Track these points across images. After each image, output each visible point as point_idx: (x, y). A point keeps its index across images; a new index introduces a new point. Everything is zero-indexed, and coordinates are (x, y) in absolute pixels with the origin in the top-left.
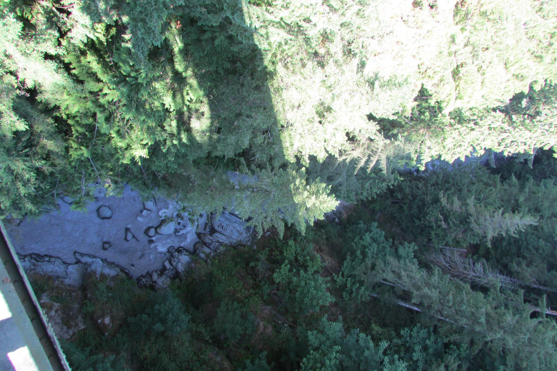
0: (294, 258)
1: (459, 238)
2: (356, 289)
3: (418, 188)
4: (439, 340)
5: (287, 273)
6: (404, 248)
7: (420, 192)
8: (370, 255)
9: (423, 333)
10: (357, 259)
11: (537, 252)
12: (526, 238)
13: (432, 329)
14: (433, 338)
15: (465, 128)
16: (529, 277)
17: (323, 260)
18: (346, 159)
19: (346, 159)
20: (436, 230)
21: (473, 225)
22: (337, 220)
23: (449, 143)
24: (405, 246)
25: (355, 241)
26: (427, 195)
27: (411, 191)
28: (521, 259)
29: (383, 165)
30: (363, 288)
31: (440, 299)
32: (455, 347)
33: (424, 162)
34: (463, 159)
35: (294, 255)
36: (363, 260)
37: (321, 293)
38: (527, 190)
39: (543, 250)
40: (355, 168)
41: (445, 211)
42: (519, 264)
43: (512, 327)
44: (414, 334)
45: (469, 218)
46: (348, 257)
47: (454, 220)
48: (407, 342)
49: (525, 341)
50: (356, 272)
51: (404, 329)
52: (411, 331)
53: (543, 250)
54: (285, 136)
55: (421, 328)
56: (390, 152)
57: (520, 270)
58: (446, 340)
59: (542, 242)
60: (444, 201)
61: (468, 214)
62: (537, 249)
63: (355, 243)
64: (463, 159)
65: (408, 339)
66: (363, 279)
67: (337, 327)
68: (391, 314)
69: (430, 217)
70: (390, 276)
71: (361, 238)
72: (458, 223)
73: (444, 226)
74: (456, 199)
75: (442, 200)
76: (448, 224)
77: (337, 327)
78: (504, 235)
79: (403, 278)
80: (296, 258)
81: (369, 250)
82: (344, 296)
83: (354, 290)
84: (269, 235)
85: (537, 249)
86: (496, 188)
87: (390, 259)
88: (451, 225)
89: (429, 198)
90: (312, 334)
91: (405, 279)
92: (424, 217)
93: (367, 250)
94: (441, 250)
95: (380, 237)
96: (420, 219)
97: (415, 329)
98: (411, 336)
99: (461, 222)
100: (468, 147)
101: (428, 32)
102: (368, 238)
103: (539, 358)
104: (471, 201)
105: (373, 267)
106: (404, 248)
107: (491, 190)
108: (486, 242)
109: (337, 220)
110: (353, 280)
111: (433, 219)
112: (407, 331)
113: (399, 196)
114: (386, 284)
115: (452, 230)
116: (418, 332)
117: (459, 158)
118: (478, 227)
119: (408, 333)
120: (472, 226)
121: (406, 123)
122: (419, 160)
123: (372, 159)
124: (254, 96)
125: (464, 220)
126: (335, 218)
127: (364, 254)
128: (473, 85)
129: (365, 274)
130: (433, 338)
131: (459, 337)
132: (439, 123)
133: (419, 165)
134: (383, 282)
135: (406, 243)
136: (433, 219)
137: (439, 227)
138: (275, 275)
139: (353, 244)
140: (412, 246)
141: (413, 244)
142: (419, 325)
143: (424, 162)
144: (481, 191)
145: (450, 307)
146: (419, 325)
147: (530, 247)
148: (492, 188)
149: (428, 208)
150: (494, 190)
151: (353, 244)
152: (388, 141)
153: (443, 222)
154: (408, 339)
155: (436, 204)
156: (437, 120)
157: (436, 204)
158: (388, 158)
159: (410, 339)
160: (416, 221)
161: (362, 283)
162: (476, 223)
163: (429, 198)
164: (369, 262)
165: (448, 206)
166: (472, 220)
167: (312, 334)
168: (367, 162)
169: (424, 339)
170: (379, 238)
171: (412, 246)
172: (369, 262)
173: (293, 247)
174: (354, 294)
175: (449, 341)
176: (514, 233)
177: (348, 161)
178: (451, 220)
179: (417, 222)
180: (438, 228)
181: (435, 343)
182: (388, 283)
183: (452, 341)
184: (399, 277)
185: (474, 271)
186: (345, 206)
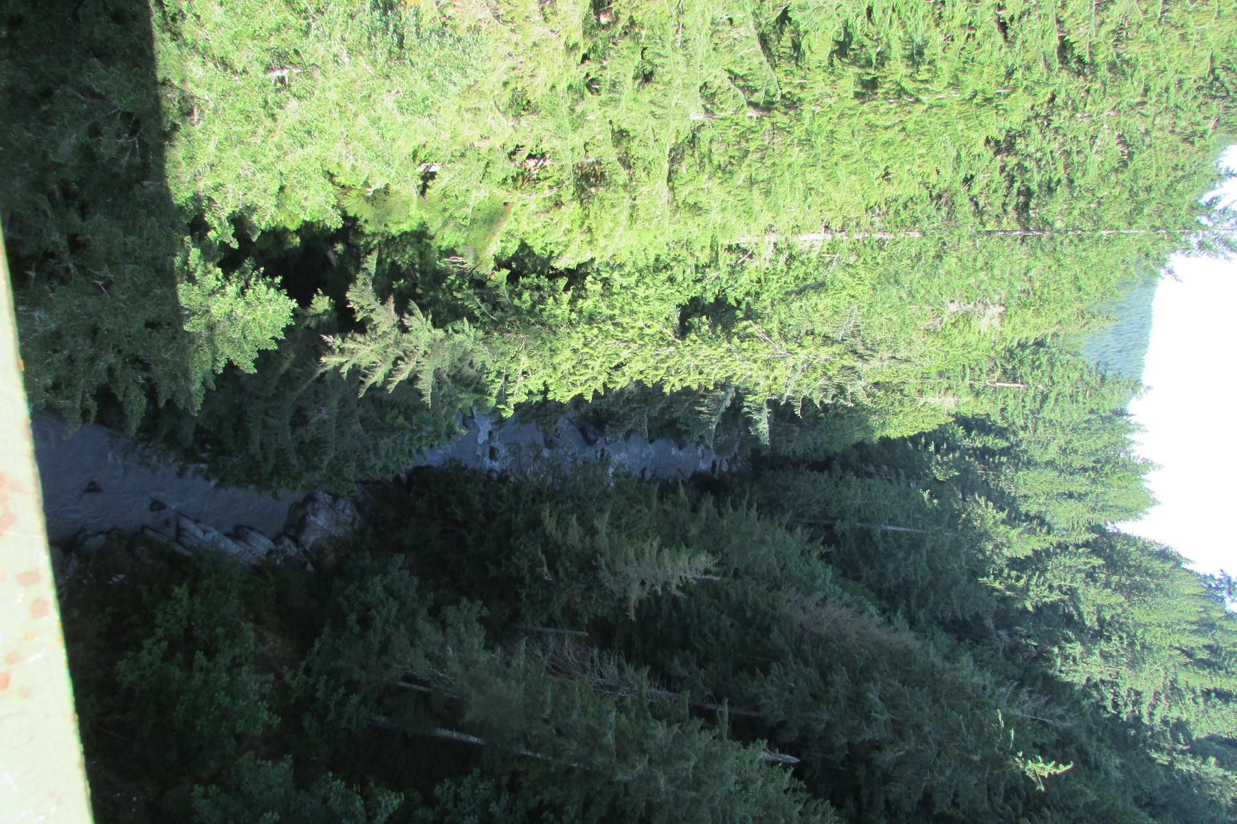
0: (181, 632)
1: (576, 603)
2: (337, 703)
3: (500, 497)
4: (519, 803)
5: (158, 664)
6: (459, 609)
7: (505, 507)
8: (378, 623)
9: (484, 788)
10: (348, 633)
11: (717, 640)
12: (699, 611)
13: (505, 780)
14: (506, 797)
15: (595, 331)
16: (702, 687)
17: (262, 640)
18: (342, 365)
19: (342, 365)
20: (530, 587)
21: (604, 574)
22: (310, 567)
23: (565, 359)
24: (461, 606)
25: (347, 592)
26: (517, 512)
27: (486, 505)
28: (688, 652)
29: (426, 384)
30: (354, 699)
31: (526, 706)
32: (552, 817)
33: (512, 401)
34: (589, 397)
35: (185, 623)
36: (361, 636)
37: (242, 703)
38: (703, 514)
39: (727, 636)
40: (362, 382)
41: (551, 546)
42: (685, 663)
43: (665, 750)
44: (465, 793)
45: (596, 560)
46: (327, 630)
47: (568, 564)
48: (448, 813)
49: (687, 777)
50: (341, 663)
51: (442, 783)
52: (459, 785)
53: (727, 636)
54: (177, 153)
55: (482, 777)
56: (444, 361)
57: (686, 673)
58: (533, 803)
59: (726, 621)
60: (550, 524)
61: (595, 551)
62: (717, 635)
63: (347, 598)
64: (589, 397)
65: (450, 806)
66: (356, 677)
67: (279, 771)
68: (415, 749)
69: (519, 559)
70: (422, 667)
71: (362, 588)
72: (575, 570)
73: (548, 577)
74: (574, 520)
75: (546, 521)
76: (556, 573)
77: (279, 771)
78: (660, 593)
79: (449, 663)
80: (189, 630)
81: (379, 613)
82: (306, 724)
83: (332, 705)
84: (122, 582)
85: (717, 635)
86: (649, 508)
87: (425, 626)
88: (561, 574)
89: (520, 520)
90: (206, 796)
91: (455, 667)
92: (508, 559)
93: (374, 612)
94: (539, 635)
95: (407, 588)
96: (497, 564)
97: (467, 781)
98: (457, 798)
99: (581, 570)
100: (599, 373)
101: (535, 44)
102: (379, 588)
103: (713, 811)
104: (602, 524)
105: (384, 648)
106: (459, 609)
107: (640, 511)
108: (627, 609)
109: (310, 567)
110: (332, 683)
111: (525, 563)
112: (449, 788)
113: (459, 514)
114: (410, 689)
115: (562, 585)
116: (474, 787)
117: (581, 395)
118: (612, 578)
119: (452, 791)
120: (601, 575)
121: (483, 314)
122: (502, 397)
123: (402, 364)
124: (104, 77)
125: (588, 564)
126: (305, 564)
127: (365, 623)
128: (615, 211)
129: (363, 667)
130: (506, 797)
131: (560, 794)
132: (549, 317)
133: (501, 407)
134: (401, 684)
135: (464, 600)
136: (525, 563)
137: (538, 578)
138: (121, 665)
139: (341, 599)
140: (476, 609)
141: (480, 603)
142: (477, 771)
143: (512, 401)
144: (622, 512)
145: (546, 721)
146: (477, 771)
147: (706, 630)
148: (643, 506)
149: (518, 538)
150: (646, 511)
151: (341, 599)
152: (440, 333)
153: (545, 569)
154: (450, 806)
155: (534, 530)
156: (544, 310)
157: (534, 530)
158: (437, 374)
159: (456, 806)
160: (491, 567)
161: (353, 687)
162: (610, 570)
163: (520, 520)
164: (375, 640)
165: (558, 536)
166: (603, 561)
167: (206, 796)
168: (389, 375)
169: (486, 803)
170: (404, 591)
171: (476, 609)
172: (375, 640)
173: (185, 602)
174: (331, 717)
175: (541, 802)
176: (678, 587)
177: (345, 369)
178: (562, 564)
179: (493, 571)
180: (535, 582)
181: (511, 812)
182: (415, 686)
183: (546, 802)
184: (441, 663)
185: (601, 676)
186: (334, 537)
